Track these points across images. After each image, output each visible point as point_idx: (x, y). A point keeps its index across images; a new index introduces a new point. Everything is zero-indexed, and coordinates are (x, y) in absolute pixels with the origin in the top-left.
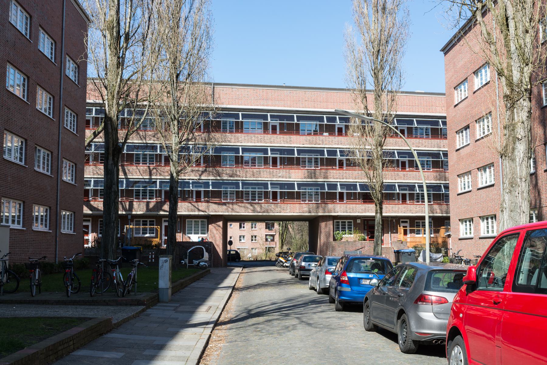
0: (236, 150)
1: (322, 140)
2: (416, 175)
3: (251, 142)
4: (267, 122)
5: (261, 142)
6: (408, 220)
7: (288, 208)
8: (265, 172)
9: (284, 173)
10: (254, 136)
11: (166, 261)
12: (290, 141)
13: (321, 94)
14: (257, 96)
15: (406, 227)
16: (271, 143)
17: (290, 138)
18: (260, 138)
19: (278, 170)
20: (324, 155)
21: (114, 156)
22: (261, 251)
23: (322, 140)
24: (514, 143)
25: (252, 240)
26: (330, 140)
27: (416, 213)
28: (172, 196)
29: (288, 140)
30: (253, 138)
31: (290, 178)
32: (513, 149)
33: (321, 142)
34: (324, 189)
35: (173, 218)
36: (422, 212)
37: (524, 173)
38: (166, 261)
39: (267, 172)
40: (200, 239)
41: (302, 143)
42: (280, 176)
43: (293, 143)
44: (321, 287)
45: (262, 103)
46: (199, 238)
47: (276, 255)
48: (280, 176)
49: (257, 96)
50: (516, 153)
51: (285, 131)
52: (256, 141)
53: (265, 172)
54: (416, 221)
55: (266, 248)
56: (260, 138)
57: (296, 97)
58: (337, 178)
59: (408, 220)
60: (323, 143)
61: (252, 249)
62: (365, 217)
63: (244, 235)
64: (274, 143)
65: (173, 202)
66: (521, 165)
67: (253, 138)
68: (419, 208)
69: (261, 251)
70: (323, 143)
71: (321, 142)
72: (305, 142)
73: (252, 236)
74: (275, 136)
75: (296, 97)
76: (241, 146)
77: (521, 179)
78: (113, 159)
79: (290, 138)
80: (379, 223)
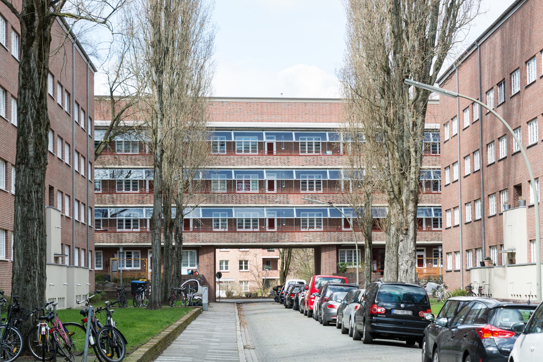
0: (228, 173)
1: (324, 160)
2: (432, 198)
3: (245, 165)
4: (263, 142)
5: (256, 164)
6: (425, 249)
7: (287, 237)
8: (260, 198)
9: (282, 198)
10: (248, 158)
11: (206, 289)
12: (288, 162)
13: (324, 105)
14: (250, 110)
15: (422, 256)
16: (267, 164)
17: (288, 159)
18: (254, 159)
19: (275, 195)
20: (326, 177)
21: (170, 228)
22: (256, 285)
23: (324, 160)
24: (390, 226)
25: (241, 268)
26: (333, 160)
27: (432, 240)
28: (177, 235)
29: (286, 161)
30: (247, 160)
31: (288, 203)
32: (390, 229)
33: (322, 163)
34: (327, 216)
35: (179, 256)
36: (439, 240)
37: (395, 242)
38: (206, 289)
39: (262, 197)
40: (190, 271)
41: (301, 164)
42: (277, 202)
43: (292, 164)
44: (212, 254)
45: (256, 118)
46: (188, 270)
47: (274, 289)
48: (277, 202)
49: (250, 110)
50: (391, 231)
51: (283, 149)
52: (250, 163)
53: (260, 198)
54: (434, 249)
55: (263, 279)
56: (254, 159)
57: (295, 110)
58: (341, 203)
59: (425, 249)
60: (325, 163)
61: (241, 282)
62: (381, 246)
63: (226, 259)
64: (270, 165)
65: (178, 241)
66: (393, 237)
67: (247, 160)
68: (435, 236)
69: (256, 285)
70: (325, 163)
71: (322, 163)
72: (305, 163)
73: (241, 262)
74: (271, 157)
75: (295, 110)
76: (234, 169)
77: (393, 245)
78: (170, 230)
79: (288, 159)
80: (369, 257)
